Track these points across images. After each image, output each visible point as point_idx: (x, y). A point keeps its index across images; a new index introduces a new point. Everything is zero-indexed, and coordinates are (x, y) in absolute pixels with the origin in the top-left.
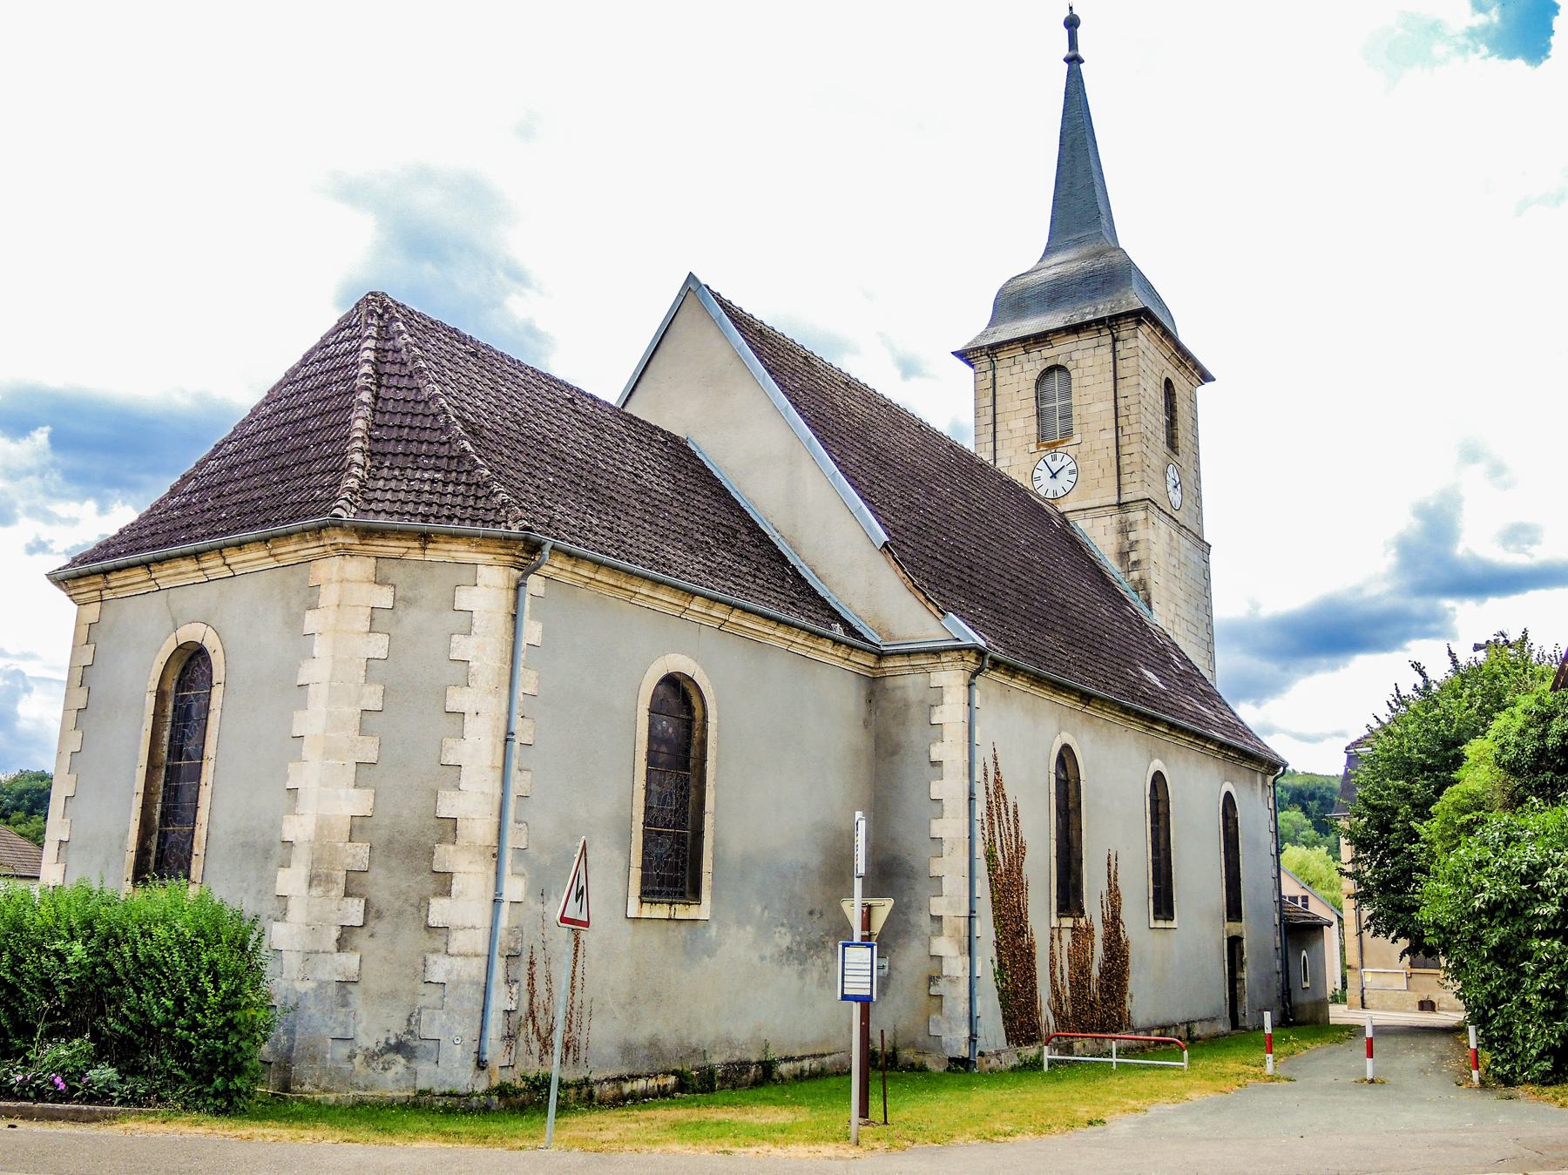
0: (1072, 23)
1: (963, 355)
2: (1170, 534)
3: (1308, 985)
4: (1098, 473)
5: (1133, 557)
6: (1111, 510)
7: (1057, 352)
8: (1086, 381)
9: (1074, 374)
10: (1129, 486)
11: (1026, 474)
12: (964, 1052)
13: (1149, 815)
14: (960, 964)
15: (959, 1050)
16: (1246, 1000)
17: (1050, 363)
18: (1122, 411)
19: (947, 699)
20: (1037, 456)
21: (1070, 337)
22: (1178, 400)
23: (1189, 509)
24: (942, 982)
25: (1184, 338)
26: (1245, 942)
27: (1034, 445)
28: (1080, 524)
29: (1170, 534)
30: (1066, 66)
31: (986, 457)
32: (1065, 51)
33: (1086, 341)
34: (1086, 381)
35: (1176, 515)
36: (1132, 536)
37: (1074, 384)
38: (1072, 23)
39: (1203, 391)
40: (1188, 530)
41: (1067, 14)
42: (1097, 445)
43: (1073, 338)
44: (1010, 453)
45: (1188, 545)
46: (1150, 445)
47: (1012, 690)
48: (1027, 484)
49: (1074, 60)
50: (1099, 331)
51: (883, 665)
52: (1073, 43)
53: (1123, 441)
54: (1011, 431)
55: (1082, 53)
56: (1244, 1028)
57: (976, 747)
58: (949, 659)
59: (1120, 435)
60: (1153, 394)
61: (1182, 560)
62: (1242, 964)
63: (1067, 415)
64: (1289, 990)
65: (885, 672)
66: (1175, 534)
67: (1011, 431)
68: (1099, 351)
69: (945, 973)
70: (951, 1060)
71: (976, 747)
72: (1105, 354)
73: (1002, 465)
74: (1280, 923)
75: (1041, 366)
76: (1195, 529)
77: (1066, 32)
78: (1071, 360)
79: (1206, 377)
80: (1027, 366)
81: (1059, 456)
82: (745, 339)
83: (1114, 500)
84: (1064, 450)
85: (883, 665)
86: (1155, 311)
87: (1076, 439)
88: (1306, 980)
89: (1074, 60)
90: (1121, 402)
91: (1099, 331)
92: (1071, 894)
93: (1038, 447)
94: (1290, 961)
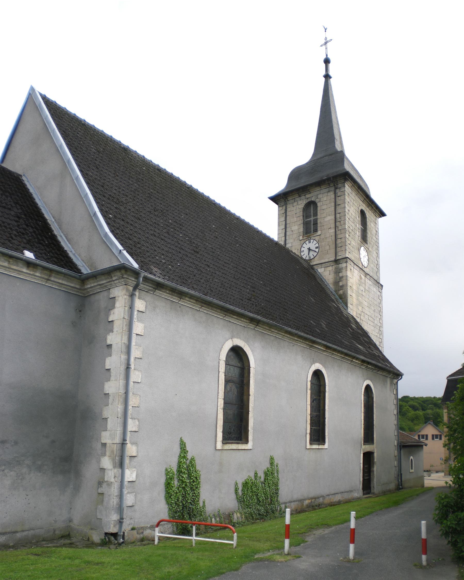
0: (327, 61)
1: (275, 199)
2: (360, 276)
3: (413, 471)
4: (327, 248)
5: (341, 284)
6: (332, 264)
7: (312, 196)
8: (324, 207)
9: (319, 204)
10: (340, 252)
11: (298, 249)
12: (113, 529)
13: (309, 392)
14: (113, 474)
15: (110, 528)
16: (375, 480)
17: (309, 200)
18: (338, 220)
19: (117, 305)
20: (303, 242)
21: (317, 188)
22: (368, 220)
23: (372, 269)
24: (104, 485)
25: (374, 196)
26: (375, 455)
27: (302, 236)
28: (319, 270)
29: (360, 276)
30: (324, 79)
31: (282, 243)
32: (324, 73)
33: (324, 190)
34: (324, 207)
35: (364, 269)
36: (341, 275)
37: (319, 209)
38: (327, 61)
39: (381, 220)
40: (371, 276)
41: (325, 57)
42: (328, 235)
43: (318, 189)
44: (291, 241)
45: (371, 283)
46: (351, 235)
47: (182, 307)
48: (299, 254)
49: (327, 77)
50: (329, 184)
51: (86, 287)
52: (327, 69)
53: (338, 232)
54: (292, 231)
55: (331, 74)
56: (374, 493)
57: (225, 360)
58: (116, 278)
59: (337, 230)
60: (354, 214)
61: (367, 288)
62: (373, 463)
63: (316, 223)
64: (401, 474)
65: (88, 292)
66: (363, 277)
67: (292, 231)
68: (329, 194)
69: (106, 479)
70: (106, 534)
71: (225, 360)
72: (332, 195)
73: (288, 246)
74: (398, 445)
75: (305, 202)
76: (376, 278)
77: (324, 65)
78: (318, 198)
79: (382, 214)
80: (300, 202)
81: (312, 241)
82: (328, 288)
83: (333, 259)
84: (314, 238)
85: (86, 287)
86: (352, 173)
87: (319, 233)
88: (412, 469)
89: (327, 77)
90: (338, 216)
91: (329, 184)
92: (243, 431)
93: (303, 237)
94: (402, 460)
